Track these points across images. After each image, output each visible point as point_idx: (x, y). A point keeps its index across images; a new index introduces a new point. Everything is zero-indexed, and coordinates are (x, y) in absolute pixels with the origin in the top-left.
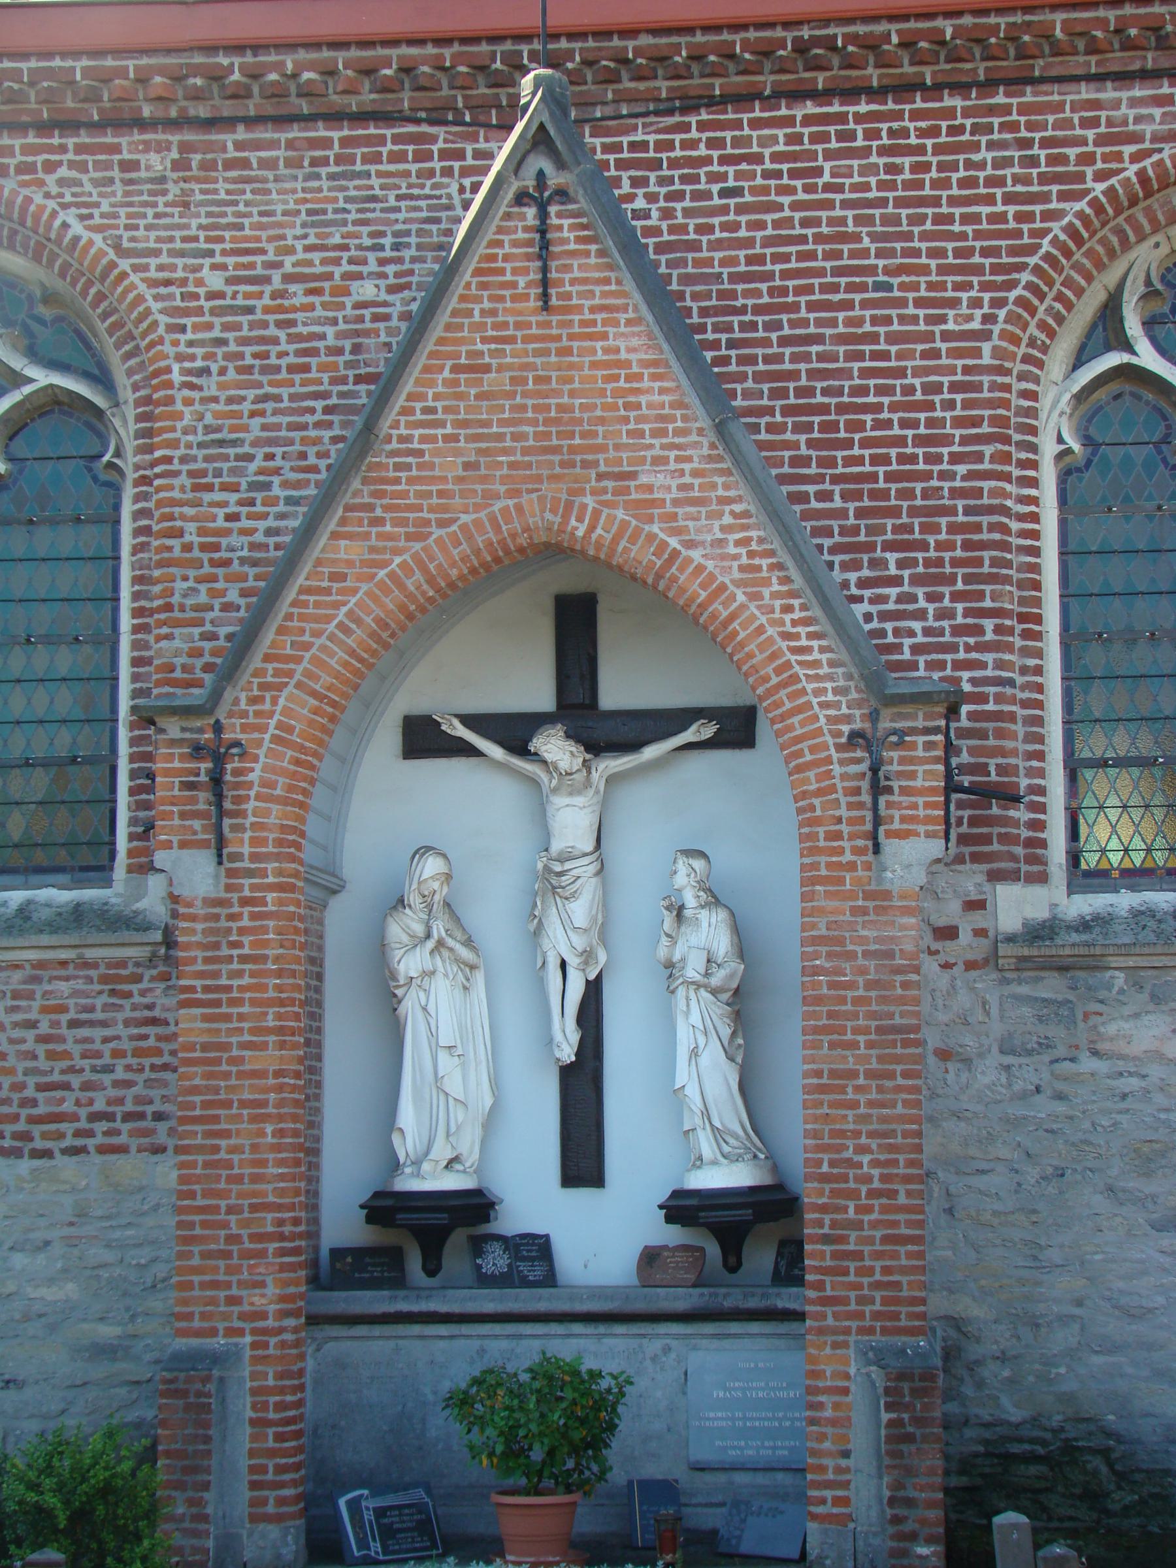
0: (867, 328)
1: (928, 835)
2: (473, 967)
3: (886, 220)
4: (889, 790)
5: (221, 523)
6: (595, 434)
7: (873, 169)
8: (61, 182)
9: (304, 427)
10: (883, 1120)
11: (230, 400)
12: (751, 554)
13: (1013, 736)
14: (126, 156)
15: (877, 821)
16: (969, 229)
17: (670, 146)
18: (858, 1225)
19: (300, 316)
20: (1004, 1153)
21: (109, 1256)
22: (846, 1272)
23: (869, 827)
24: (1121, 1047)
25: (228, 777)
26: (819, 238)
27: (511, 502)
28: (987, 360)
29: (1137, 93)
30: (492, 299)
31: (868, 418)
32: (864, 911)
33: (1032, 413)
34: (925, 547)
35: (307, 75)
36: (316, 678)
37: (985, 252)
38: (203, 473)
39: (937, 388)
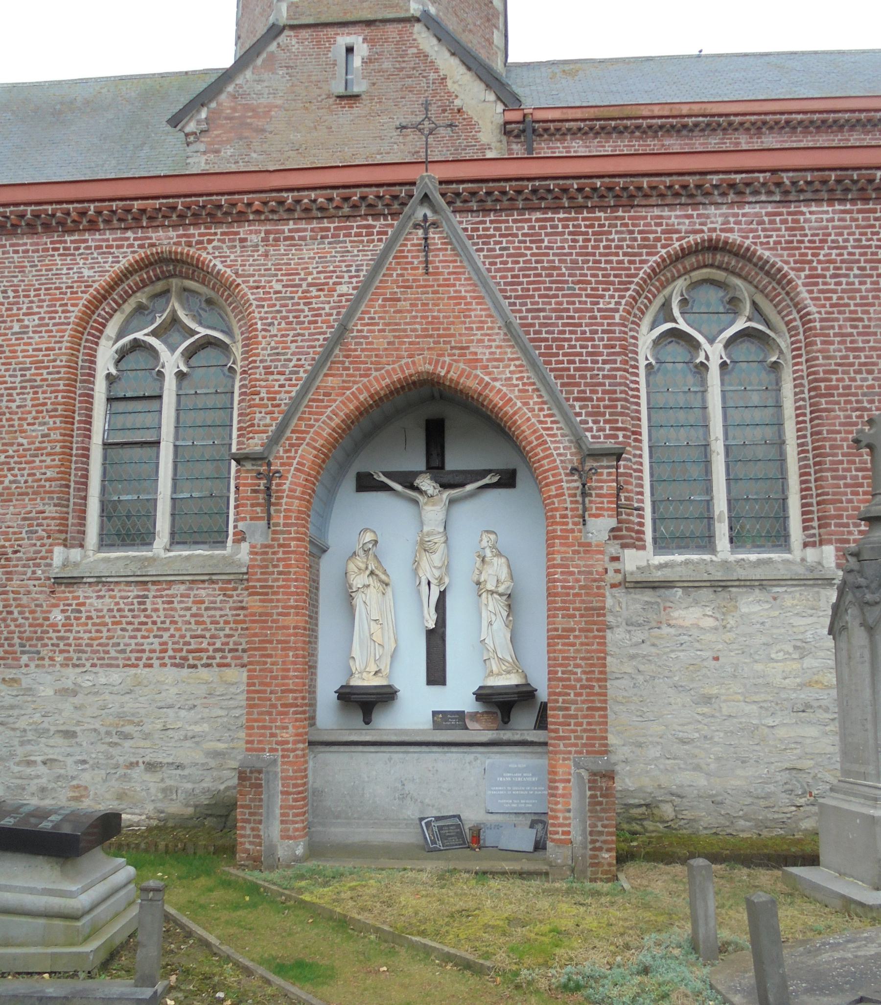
0: (565, 306)
1: (609, 516)
2: (387, 585)
3: (572, 262)
4: (591, 495)
5: (277, 388)
6: (449, 329)
7: (566, 241)
8: (214, 248)
9: (314, 347)
10: (588, 651)
11: (283, 336)
12: (524, 384)
13: (631, 484)
14: (242, 236)
15: (585, 509)
16: (608, 266)
17: (477, 230)
18: (575, 702)
19: (314, 300)
20: (629, 670)
21: (222, 713)
22: (569, 725)
23: (580, 512)
24: (680, 622)
25: (273, 487)
26: (543, 268)
27: (410, 360)
28: (617, 320)
29: (678, 213)
30: (402, 269)
31: (566, 344)
32: (578, 552)
33: (636, 345)
34: (591, 400)
35: (320, 200)
36: (316, 441)
37: (615, 276)
38: (270, 367)
39: (596, 332)
